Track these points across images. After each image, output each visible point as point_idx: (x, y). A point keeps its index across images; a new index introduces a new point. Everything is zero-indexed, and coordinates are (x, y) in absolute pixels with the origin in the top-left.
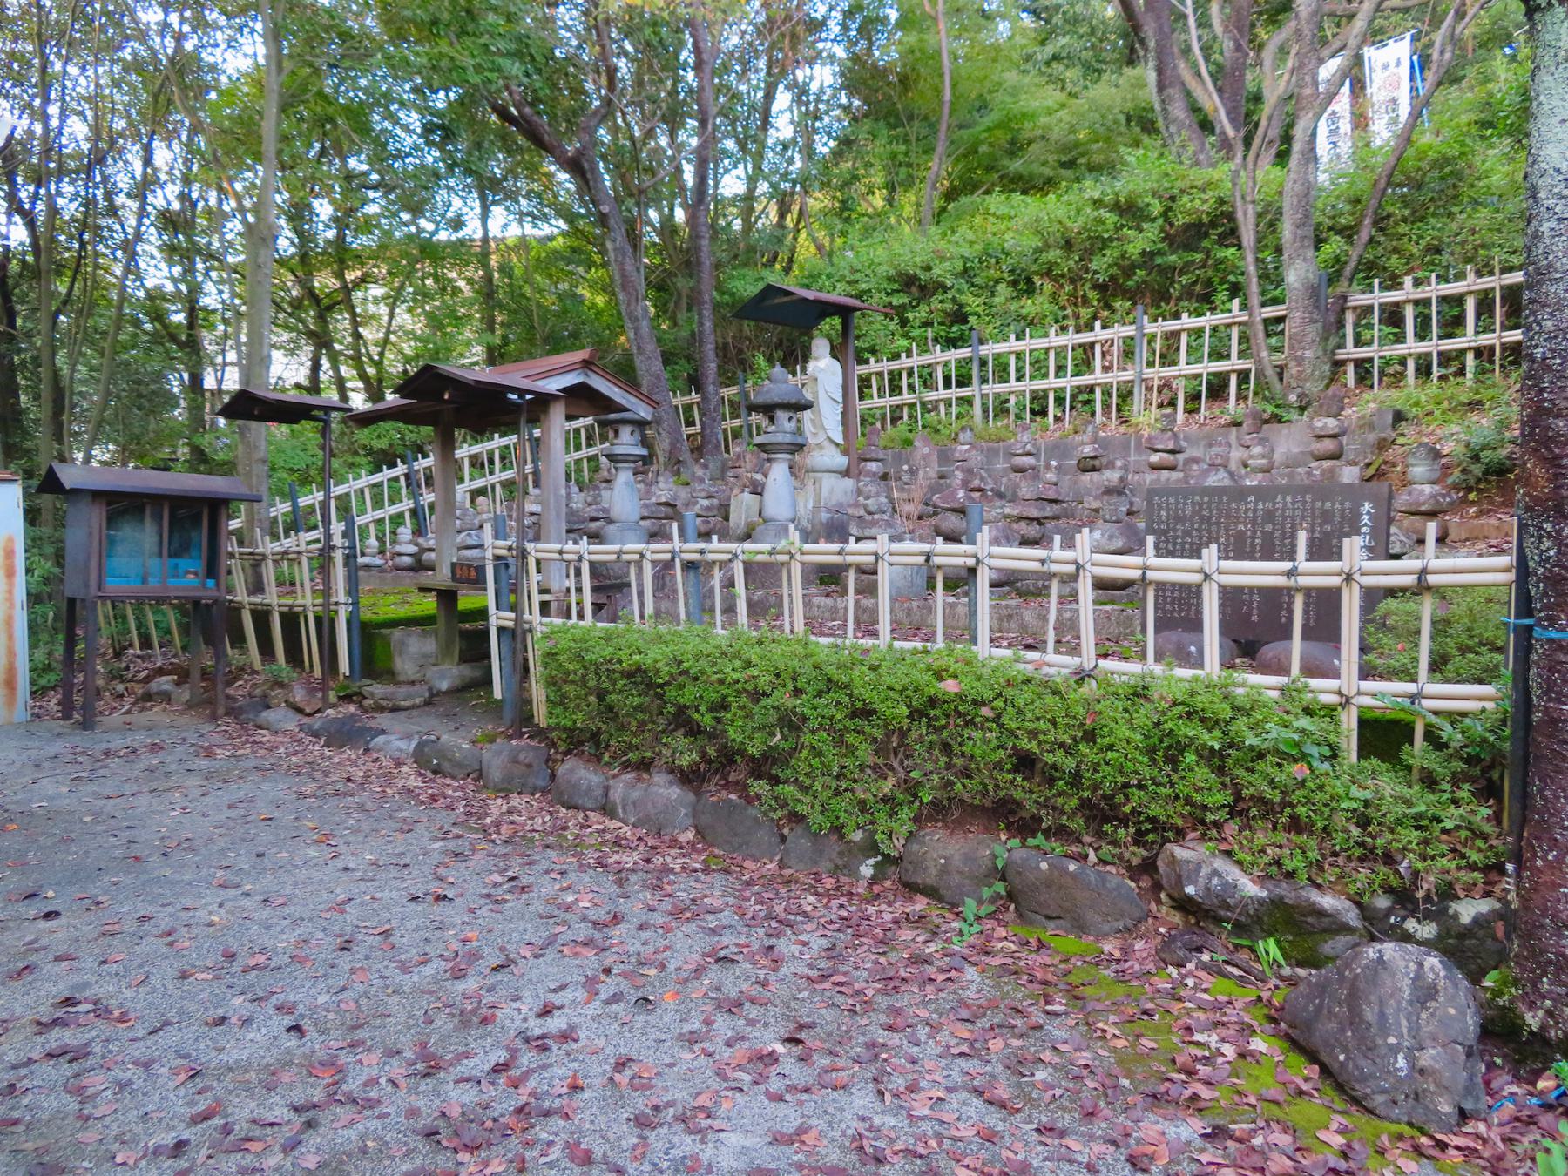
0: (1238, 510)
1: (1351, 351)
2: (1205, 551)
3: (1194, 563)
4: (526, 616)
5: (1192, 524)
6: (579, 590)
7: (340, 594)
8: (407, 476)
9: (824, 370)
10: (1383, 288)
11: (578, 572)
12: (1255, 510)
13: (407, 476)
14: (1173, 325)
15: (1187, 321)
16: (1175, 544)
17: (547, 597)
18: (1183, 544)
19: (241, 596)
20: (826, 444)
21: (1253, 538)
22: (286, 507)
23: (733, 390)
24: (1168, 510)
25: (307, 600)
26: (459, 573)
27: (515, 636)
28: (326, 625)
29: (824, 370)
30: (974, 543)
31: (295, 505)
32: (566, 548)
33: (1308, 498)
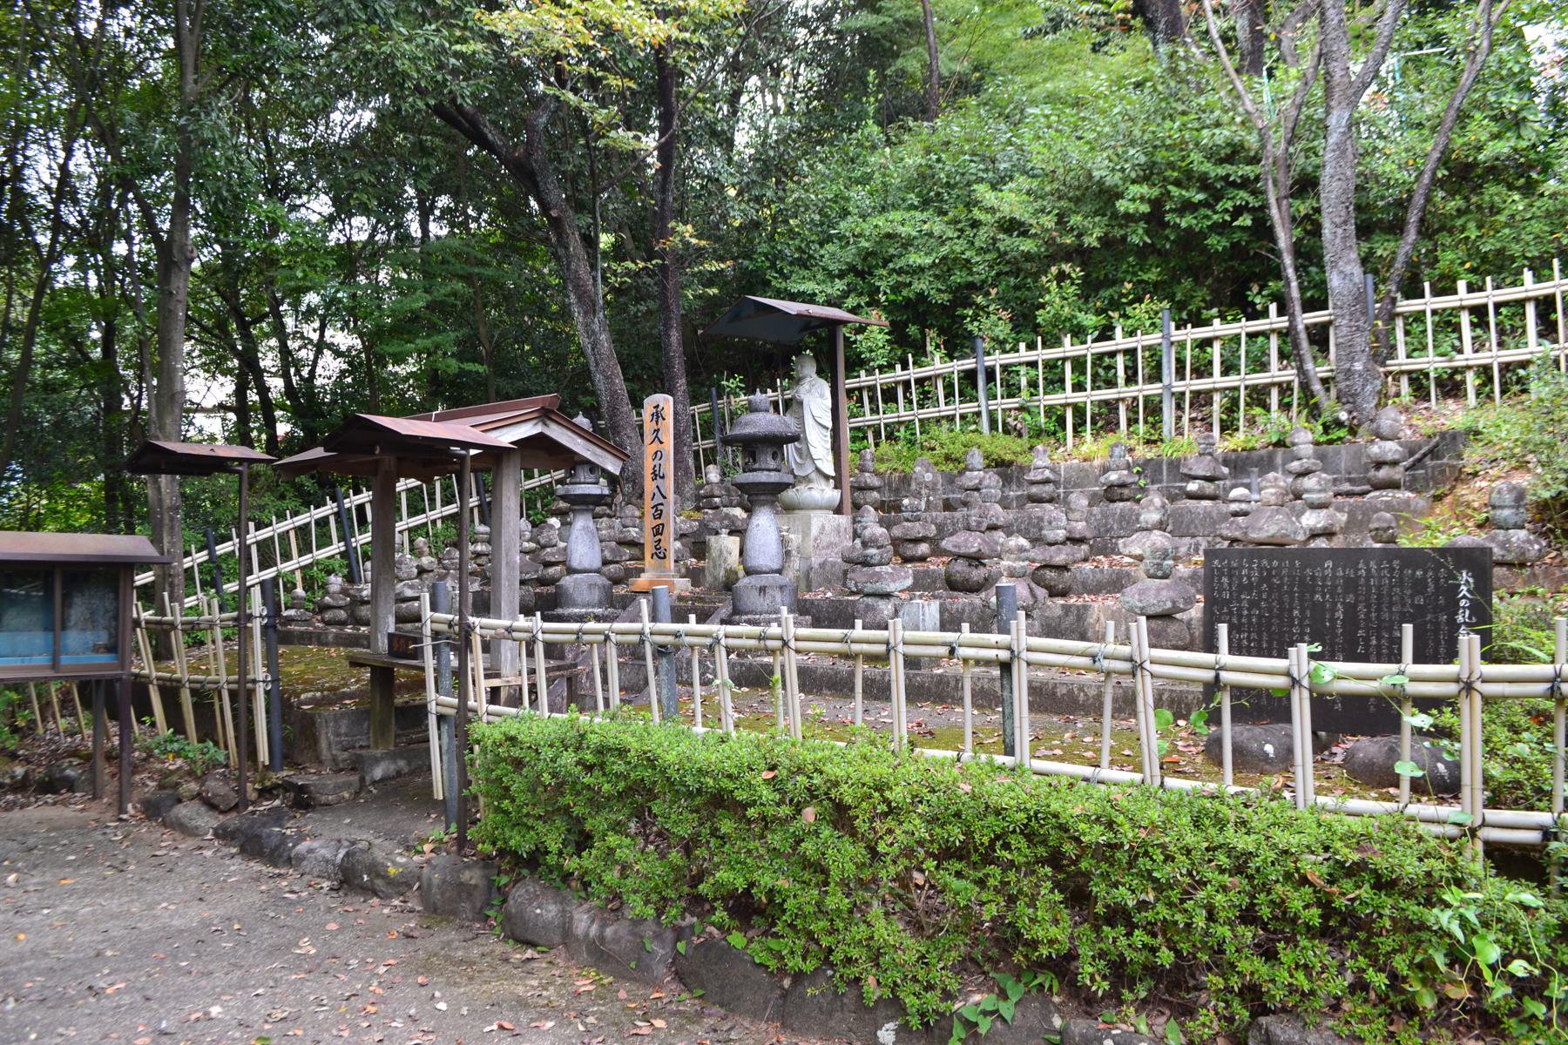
0: (1313, 578)
1: (1401, 361)
2: (1292, 650)
3: (1280, 663)
4: (471, 703)
5: (1260, 593)
6: (532, 672)
7: (260, 672)
8: (337, 515)
9: (816, 397)
10: (1437, 292)
11: (531, 654)
12: (1334, 577)
13: (337, 515)
14: (1203, 333)
15: (1218, 328)
16: (1240, 616)
17: (495, 682)
18: (1249, 616)
19: (146, 666)
20: (814, 476)
21: (1334, 610)
22: (202, 556)
23: (704, 407)
24: (1230, 577)
25: (221, 675)
26: (396, 645)
27: (460, 722)
28: (242, 697)
29: (816, 397)
30: (1007, 632)
31: (211, 554)
32: (516, 624)
33: (1396, 563)
